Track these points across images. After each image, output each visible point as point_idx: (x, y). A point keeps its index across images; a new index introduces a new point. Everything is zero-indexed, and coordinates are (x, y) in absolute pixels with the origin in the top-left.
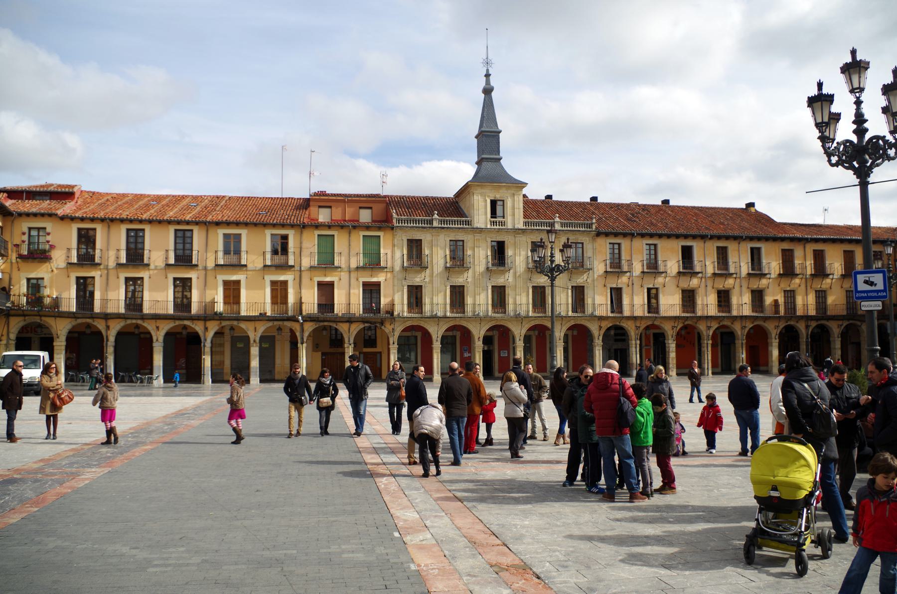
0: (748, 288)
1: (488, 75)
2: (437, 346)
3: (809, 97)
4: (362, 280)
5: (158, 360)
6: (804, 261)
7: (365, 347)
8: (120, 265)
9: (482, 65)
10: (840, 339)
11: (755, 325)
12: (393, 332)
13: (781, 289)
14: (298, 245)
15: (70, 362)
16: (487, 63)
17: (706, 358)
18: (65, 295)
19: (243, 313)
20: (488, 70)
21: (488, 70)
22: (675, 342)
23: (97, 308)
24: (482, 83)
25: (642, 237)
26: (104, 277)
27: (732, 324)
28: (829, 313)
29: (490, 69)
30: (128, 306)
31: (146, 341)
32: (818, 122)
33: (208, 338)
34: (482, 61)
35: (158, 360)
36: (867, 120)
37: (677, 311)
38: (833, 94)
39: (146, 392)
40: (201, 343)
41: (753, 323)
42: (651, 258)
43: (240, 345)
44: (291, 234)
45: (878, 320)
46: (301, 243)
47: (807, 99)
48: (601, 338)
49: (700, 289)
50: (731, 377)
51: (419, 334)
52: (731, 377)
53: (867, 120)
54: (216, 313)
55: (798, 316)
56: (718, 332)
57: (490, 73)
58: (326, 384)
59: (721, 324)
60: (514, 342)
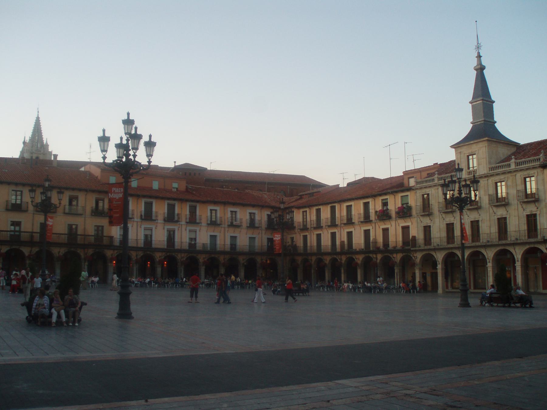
1: (479, 57)
3: (145, 141)
5: (135, 274)
8: (329, 226)
11: (354, 259)
15: (306, 286)
16: (478, 47)
17: (396, 277)
18: (455, 222)
20: (479, 53)
21: (479, 53)
25: (233, 205)
28: (218, 249)
32: (148, 154)
35: (135, 274)
36: (452, 147)
38: (156, 142)
43: (424, 275)
47: (144, 142)
53: (452, 147)
55: (130, 247)
57: (481, 55)
58: (5, 279)
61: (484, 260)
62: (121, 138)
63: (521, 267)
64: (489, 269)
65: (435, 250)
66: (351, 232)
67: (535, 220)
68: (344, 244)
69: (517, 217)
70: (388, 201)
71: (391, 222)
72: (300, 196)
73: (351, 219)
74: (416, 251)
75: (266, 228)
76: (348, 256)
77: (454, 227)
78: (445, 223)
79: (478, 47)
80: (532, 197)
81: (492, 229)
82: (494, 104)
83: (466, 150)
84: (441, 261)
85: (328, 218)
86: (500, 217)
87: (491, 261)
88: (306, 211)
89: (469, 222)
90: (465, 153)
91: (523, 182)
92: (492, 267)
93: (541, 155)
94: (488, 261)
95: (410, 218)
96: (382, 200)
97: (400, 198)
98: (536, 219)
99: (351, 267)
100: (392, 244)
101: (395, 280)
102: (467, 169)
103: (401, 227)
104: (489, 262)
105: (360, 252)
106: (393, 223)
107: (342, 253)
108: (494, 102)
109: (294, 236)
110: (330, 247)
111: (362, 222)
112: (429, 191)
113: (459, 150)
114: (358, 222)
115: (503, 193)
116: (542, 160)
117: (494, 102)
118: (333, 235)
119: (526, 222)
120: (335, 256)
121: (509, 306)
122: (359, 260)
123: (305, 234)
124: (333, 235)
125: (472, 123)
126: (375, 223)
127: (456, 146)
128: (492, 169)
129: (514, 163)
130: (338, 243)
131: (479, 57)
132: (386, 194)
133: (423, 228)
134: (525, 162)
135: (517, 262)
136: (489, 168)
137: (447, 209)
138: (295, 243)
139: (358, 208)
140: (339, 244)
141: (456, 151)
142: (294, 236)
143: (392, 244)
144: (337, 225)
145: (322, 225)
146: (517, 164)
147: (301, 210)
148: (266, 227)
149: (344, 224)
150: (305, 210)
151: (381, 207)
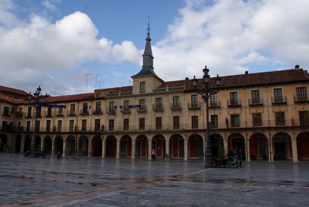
0: (273, 112)
1: (149, 34)
2: (150, 143)
4: (95, 118)
6: (104, 106)
7: (101, 155)
8: (46, 116)
9: (147, 31)
10: (296, 141)
12: (104, 138)
13: (297, 111)
14: (78, 108)
16: (149, 29)
19: (62, 131)
20: (149, 32)
21: (149, 32)
22: (227, 142)
23: (30, 131)
24: (146, 37)
26: (53, 120)
27: (263, 132)
29: (149, 31)
30: (83, 129)
31: (145, 140)
33: (65, 139)
34: (151, 30)
37: (171, 128)
39: (113, 158)
40: (203, 141)
41: (277, 131)
42: (231, 97)
44: (76, 104)
45: (235, 127)
46: (78, 106)
48: (187, 141)
49: (242, 114)
50: (57, 155)
51: (232, 138)
52: (57, 155)
54: (61, 132)
56: (232, 138)
57: (150, 33)
59: (255, 132)
60: (148, 142)
61: (115, 141)
62: (36, 91)
63: (119, 145)
64: (133, 145)
65: (146, 132)
66: (61, 121)
67: (113, 123)
68: (56, 128)
69: (168, 118)
70: (101, 104)
71: (89, 116)
72: (25, 99)
73: (30, 115)
74: (103, 134)
75: (3, 115)
76: (58, 135)
77: (129, 121)
78: (155, 117)
79: (149, 29)
80: (143, 109)
81: (152, 123)
82: (153, 59)
83: (140, 80)
84: (119, 139)
85: (26, 113)
86: (158, 117)
87: (119, 141)
88: (74, 105)
89: (139, 119)
90: (139, 81)
91: (173, 99)
92: (105, 144)
93: (184, 86)
94: (117, 141)
95: (214, 110)
96: (84, 103)
97: (95, 103)
98: (179, 119)
99: (126, 141)
100: (88, 129)
101: (177, 151)
102: (139, 90)
103: (81, 120)
104: (133, 141)
105: (90, 133)
106: (90, 117)
107: (54, 132)
108: (153, 58)
109: (21, 121)
110: (45, 129)
111: (69, 115)
112: (179, 95)
113: (136, 79)
114: (44, 116)
115: (307, 95)
116: (184, 88)
117: (153, 58)
118: (49, 122)
119: (173, 120)
120: (49, 135)
121: (220, 167)
122: (65, 137)
123: (20, 121)
124: (49, 122)
125: (142, 66)
126: (78, 116)
127: (133, 77)
128: (154, 91)
129: (168, 89)
130: (51, 127)
131: (149, 34)
132: (86, 100)
133: (109, 121)
134: (178, 89)
135: (166, 142)
136: (153, 90)
137: (110, 112)
138: (21, 126)
139: (79, 107)
140: (53, 127)
141: (133, 80)
142: (21, 121)
143: (88, 129)
144: (52, 116)
145: (52, 115)
146: (169, 89)
147: (28, 106)
148: (3, 114)
149: (57, 116)
150: (20, 107)
151: (82, 107)
